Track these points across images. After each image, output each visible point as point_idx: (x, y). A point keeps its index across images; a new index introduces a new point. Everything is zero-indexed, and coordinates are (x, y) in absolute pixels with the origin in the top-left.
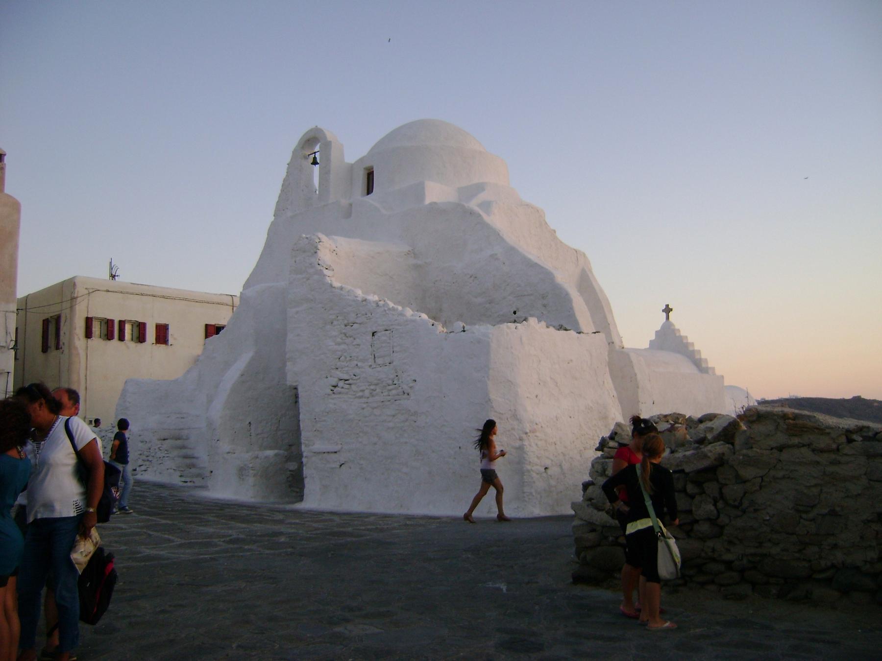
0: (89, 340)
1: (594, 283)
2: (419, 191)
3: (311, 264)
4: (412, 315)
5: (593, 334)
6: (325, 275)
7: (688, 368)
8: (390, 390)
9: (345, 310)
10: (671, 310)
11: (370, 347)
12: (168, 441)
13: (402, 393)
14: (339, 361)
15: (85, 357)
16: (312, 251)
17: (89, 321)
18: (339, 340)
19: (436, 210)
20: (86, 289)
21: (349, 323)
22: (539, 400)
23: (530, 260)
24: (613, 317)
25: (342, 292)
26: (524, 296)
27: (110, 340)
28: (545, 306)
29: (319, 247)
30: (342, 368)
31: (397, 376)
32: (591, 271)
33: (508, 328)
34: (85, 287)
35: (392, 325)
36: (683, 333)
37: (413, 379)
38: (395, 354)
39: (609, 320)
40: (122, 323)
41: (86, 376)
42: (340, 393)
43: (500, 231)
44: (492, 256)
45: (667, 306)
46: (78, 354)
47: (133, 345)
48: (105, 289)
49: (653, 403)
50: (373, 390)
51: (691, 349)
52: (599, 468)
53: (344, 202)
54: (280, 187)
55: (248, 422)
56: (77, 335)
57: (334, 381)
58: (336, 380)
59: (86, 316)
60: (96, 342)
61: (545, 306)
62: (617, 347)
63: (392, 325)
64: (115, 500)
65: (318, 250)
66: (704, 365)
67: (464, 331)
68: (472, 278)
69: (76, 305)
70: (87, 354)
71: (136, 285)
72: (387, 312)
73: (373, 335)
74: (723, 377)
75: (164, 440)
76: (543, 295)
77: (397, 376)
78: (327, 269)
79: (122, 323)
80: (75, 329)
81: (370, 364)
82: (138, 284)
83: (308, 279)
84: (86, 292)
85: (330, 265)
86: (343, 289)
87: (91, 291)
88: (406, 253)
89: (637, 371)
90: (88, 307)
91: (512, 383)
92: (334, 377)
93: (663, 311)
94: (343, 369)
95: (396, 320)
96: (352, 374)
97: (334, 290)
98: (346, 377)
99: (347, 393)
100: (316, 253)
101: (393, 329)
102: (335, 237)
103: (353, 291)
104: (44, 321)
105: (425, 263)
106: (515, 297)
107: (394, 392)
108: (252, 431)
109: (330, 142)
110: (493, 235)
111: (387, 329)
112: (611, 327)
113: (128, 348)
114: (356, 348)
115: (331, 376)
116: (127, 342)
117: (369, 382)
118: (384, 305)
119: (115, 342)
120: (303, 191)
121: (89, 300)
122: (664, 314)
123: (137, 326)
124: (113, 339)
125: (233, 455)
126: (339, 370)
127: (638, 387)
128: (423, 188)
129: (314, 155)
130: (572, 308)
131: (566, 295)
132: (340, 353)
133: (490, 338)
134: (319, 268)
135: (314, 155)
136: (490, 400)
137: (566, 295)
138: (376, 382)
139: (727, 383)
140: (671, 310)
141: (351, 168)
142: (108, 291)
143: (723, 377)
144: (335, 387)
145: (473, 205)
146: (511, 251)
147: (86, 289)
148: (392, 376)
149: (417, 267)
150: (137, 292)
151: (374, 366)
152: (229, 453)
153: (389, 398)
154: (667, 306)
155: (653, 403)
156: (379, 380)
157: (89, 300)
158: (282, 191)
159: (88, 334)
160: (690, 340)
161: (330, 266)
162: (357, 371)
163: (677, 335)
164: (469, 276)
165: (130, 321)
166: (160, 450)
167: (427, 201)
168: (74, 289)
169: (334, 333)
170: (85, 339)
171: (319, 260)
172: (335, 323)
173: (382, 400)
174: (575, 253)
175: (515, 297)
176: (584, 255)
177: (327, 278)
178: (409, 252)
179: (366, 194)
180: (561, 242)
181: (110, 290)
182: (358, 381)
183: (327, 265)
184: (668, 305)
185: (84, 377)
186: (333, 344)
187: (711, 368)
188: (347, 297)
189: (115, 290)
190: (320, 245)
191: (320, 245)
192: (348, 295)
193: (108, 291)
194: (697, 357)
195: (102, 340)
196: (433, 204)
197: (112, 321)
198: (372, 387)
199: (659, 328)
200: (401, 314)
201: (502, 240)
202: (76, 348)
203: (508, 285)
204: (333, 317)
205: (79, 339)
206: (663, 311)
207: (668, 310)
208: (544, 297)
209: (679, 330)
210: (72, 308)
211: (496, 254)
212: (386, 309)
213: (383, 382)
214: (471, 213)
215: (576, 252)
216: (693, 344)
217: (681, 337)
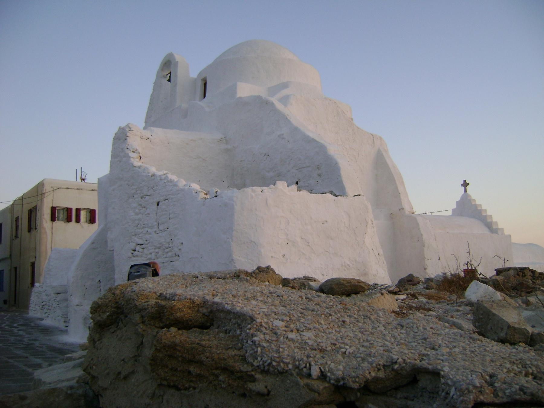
0: (53, 222)
1: (388, 161)
2: (233, 90)
3: (122, 149)
4: (185, 185)
6: (130, 157)
7: (480, 229)
8: (167, 253)
9: (141, 185)
10: (468, 184)
11: (155, 215)
12: (62, 294)
13: (175, 255)
14: (137, 229)
15: (51, 234)
17: (53, 209)
18: (137, 211)
19: (243, 103)
20: (52, 187)
21: (143, 196)
22: (287, 260)
23: (308, 136)
24: (404, 188)
26: (304, 168)
27: (69, 222)
28: (319, 175)
29: (128, 134)
30: (139, 235)
31: (171, 240)
32: (386, 151)
33: (254, 191)
34: (51, 186)
35: (168, 195)
36: (478, 202)
37: (181, 242)
38: (171, 221)
39: (400, 189)
40: (78, 211)
41: (51, 248)
42: (137, 256)
43: (288, 115)
45: (465, 181)
46: (46, 232)
47: (86, 225)
48: (65, 187)
49: (439, 259)
50: (157, 253)
51: (484, 214)
52: (513, 293)
54: (148, 101)
55: (97, 280)
56: (45, 219)
57: (133, 246)
58: (134, 244)
59: (52, 206)
60: (59, 224)
61: (319, 175)
62: (407, 213)
63: (168, 195)
64: (414, 293)
65: (127, 137)
66: (494, 227)
67: (216, 196)
68: (266, 157)
69: (44, 198)
70: (52, 232)
71: (88, 184)
72: (166, 184)
73: (158, 205)
74: (510, 236)
75: (58, 294)
76: (318, 166)
77: (171, 240)
78: (134, 152)
79: (78, 211)
80: (44, 215)
81: (155, 230)
82: (90, 183)
83: (120, 162)
84: (52, 189)
85: (137, 149)
86: (141, 168)
87: (55, 188)
88: (218, 140)
89: (422, 232)
90: (53, 200)
91: (255, 244)
92: (133, 243)
93: (462, 185)
94: (140, 235)
95: (171, 190)
96: (144, 239)
97: (134, 168)
98: (141, 242)
99: (141, 256)
100: (126, 139)
101: (170, 198)
102: (152, 128)
103: (147, 168)
104: (29, 210)
105: (234, 147)
107: (170, 254)
108: (102, 288)
109: (178, 62)
110: (284, 119)
111: (166, 199)
112: (402, 196)
113: (83, 227)
114: (147, 217)
115: (132, 242)
116: (82, 223)
117: (155, 246)
118: (165, 178)
119: (73, 223)
120: (162, 102)
121: (53, 195)
122: (463, 188)
123: (66, 210)
124: (71, 222)
125: (81, 307)
126: (137, 236)
127: (424, 246)
128: (236, 88)
130: (340, 176)
131: (335, 164)
132: (137, 222)
134: (127, 151)
136: (233, 260)
137: (335, 164)
138: (159, 245)
139: (514, 240)
140: (468, 184)
141: (195, 81)
142: (68, 188)
143: (510, 236)
144: (135, 250)
146: (296, 130)
147: (52, 187)
148: (168, 240)
150: (89, 189)
151: (158, 232)
152: (78, 305)
153: (167, 259)
154: (465, 181)
155: (439, 259)
156: (161, 244)
157: (53, 195)
158: (150, 103)
159: (53, 218)
160: (484, 207)
161: (137, 150)
162: (148, 237)
163: (473, 203)
165: (84, 209)
166: (55, 302)
167: (238, 96)
168: (43, 187)
169: (135, 205)
170: (51, 222)
171: (128, 145)
172: (136, 196)
173: (163, 262)
174: (371, 136)
176: (381, 138)
177: (132, 159)
178: (221, 139)
180: (358, 128)
181: (69, 187)
182: (148, 245)
183: (134, 149)
184: (466, 180)
185: (50, 249)
186: (133, 214)
187: (500, 229)
188: (143, 174)
189: (73, 187)
190: (129, 133)
191: (129, 133)
192: (144, 173)
193: (68, 188)
194: (489, 220)
195: (63, 223)
196: (241, 98)
197: (71, 209)
198: (157, 250)
199: (459, 199)
201: (289, 122)
202: (44, 229)
203: (291, 160)
204: (133, 191)
205: (47, 222)
206: (462, 185)
207: (465, 184)
208: (318, 168)
209: (474, 200)
210: (42, 200)
212: (165, 181)
213: (163, 245)
214: (267, 103)
216: (485, 210)
217: (476, 205)
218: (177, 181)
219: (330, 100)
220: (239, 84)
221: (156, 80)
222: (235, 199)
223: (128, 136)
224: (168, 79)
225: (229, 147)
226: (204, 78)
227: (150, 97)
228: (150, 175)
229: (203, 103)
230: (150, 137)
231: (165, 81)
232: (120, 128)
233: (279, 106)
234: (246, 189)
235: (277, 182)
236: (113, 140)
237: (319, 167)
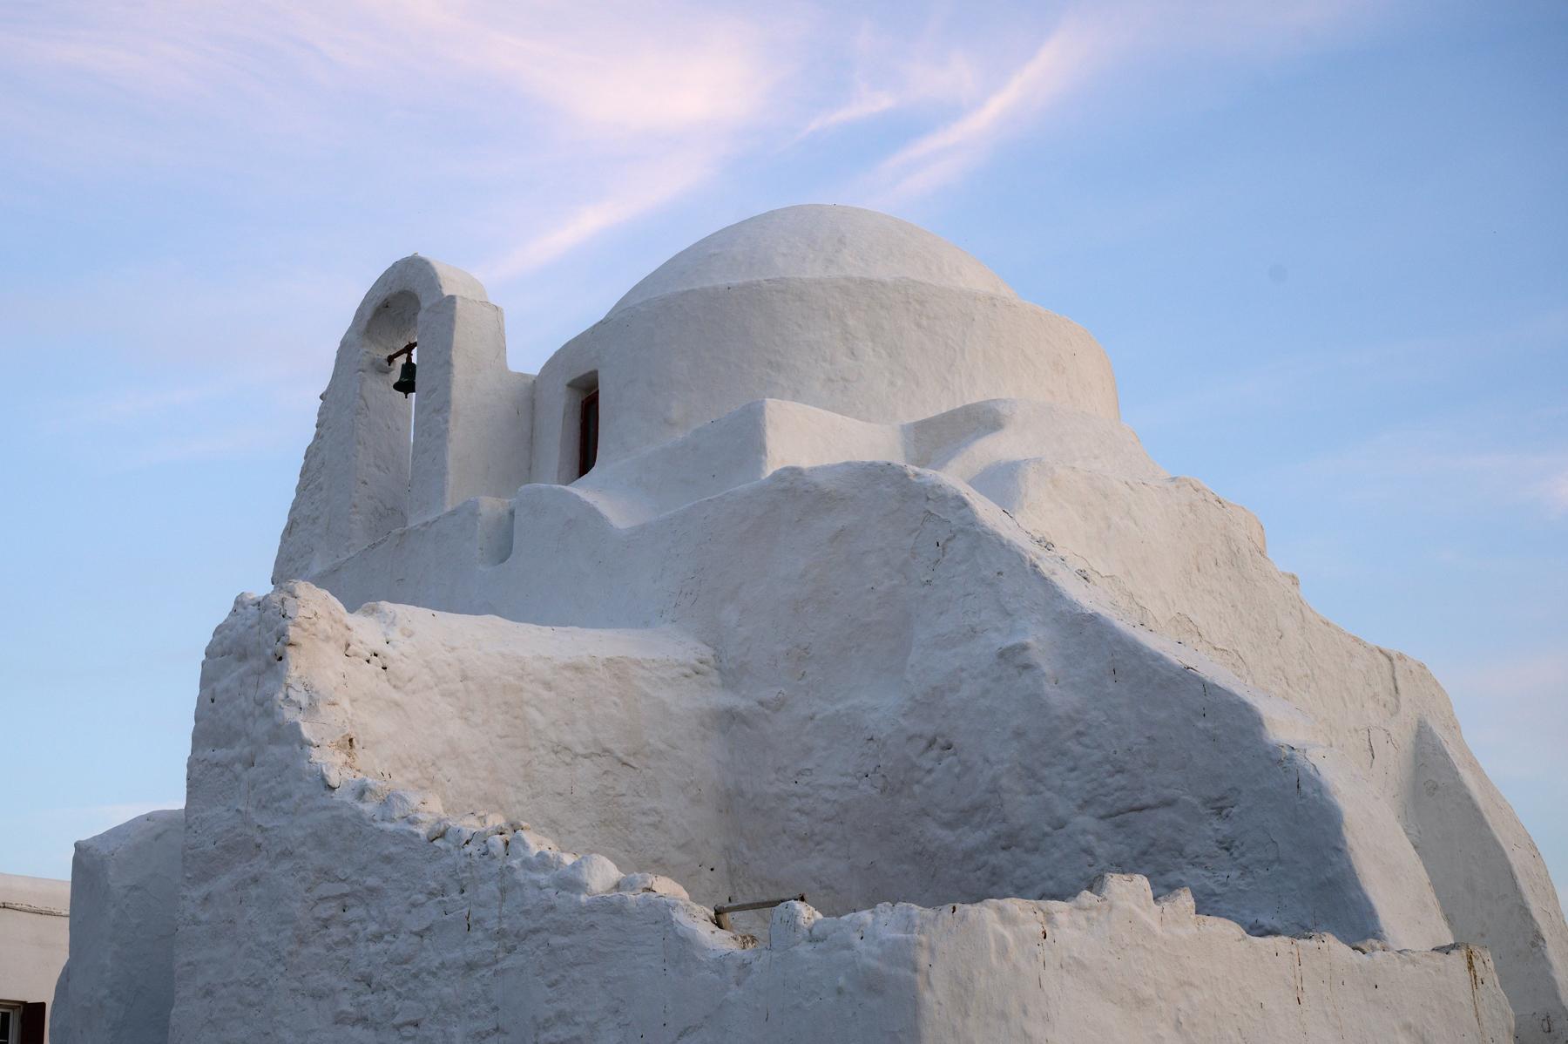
4: (618, 886)
5: (1437, 955)
16: (269, 651)
23: (1158, 658)
25: (361, 806)
44: (1004, 655)
53: (490, 506)
68: (934, 753)
88: (688, 671)
106: (1102, 818)
109: (452, 299)
129: (406, 355)
133: (915, 970)
135: (406, 355)
141: (530, 394)
145: (952, 477)
149: (729, 719)
164: (924, 743)
167: (771, 468)
175: (1102, 818)
177: (315, 753)
179: (577, 470)
188: (381, 825)
196: (793, 474)
200: (571, 883)
211: (1025, 648)
215: (1391, 660)
218: (574, 866)
219: (1197, 490)
220: (771, 403)
221: (334, 376)
222: (923, 959)
223: (292, 640)
224: (396, 376)
225: (740, 702)
226: (591, 373)
227: (302, 461)
228: (422, 831)
229: (584, 490)
230: (379, 645)
231: (383, 388)
232: (239, 602)
233: (986, 510)
234: (972, 910)
235: (1108, 875)
236: (203, 657)
237: (1222, 808)
